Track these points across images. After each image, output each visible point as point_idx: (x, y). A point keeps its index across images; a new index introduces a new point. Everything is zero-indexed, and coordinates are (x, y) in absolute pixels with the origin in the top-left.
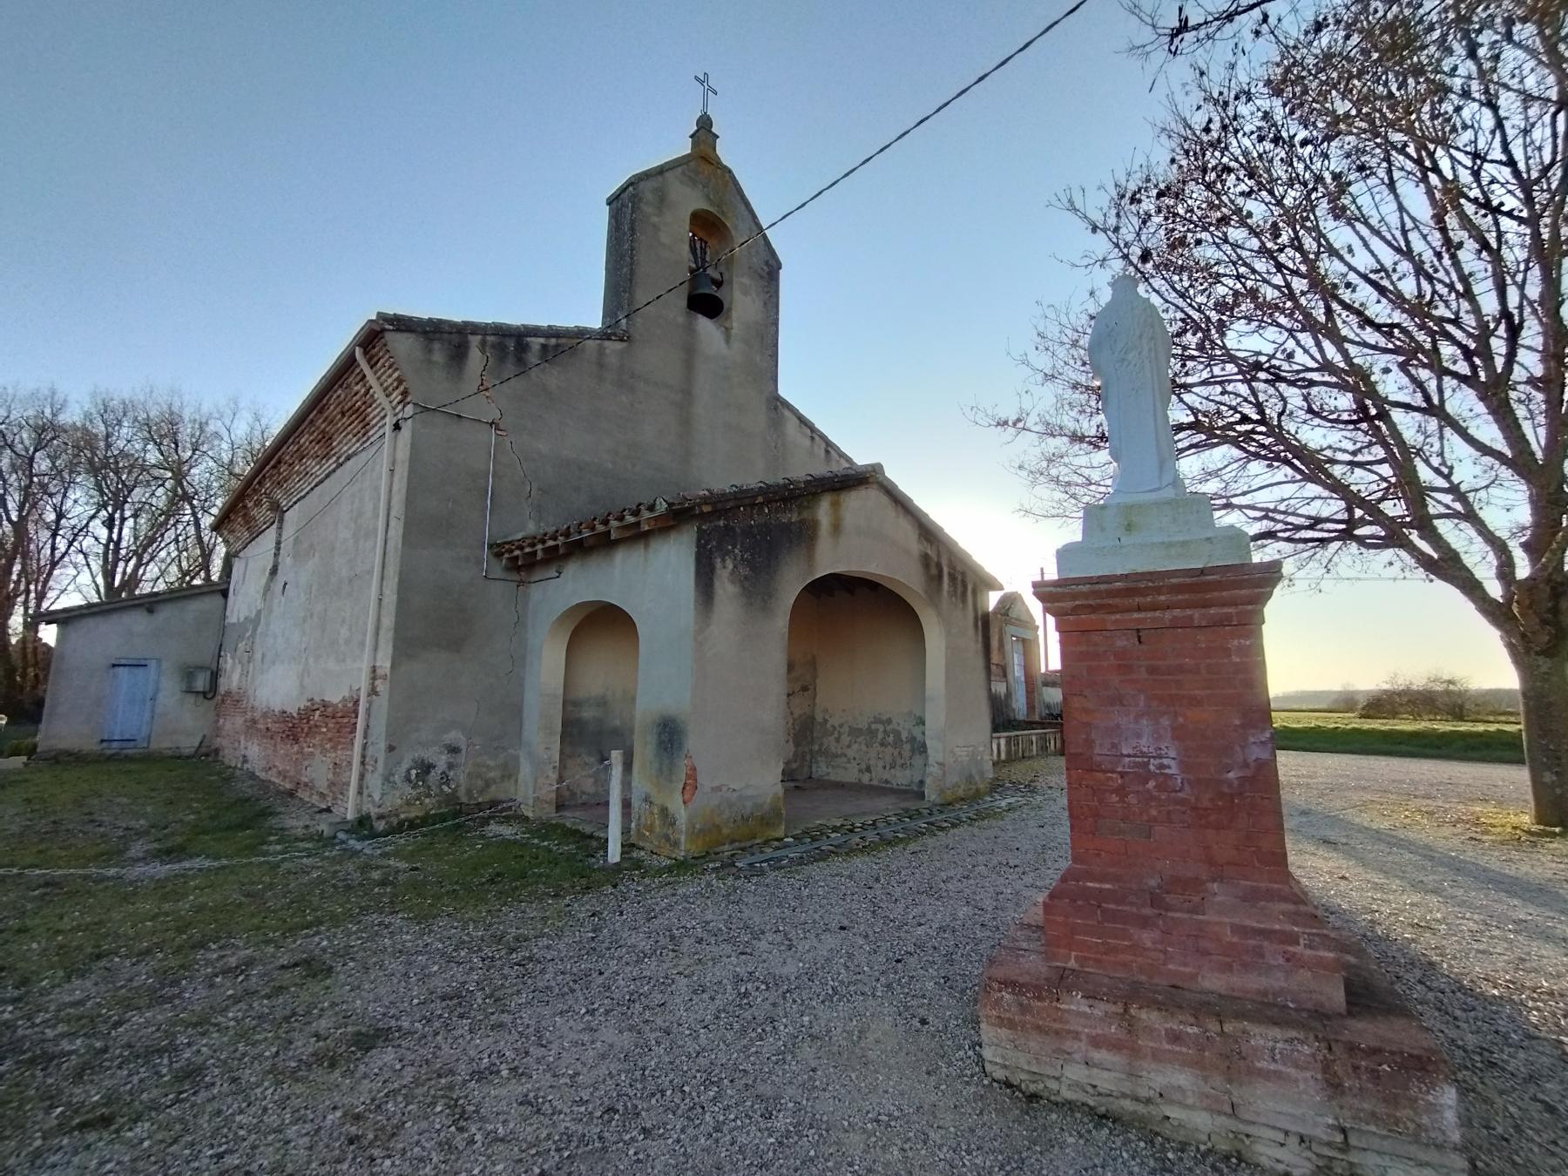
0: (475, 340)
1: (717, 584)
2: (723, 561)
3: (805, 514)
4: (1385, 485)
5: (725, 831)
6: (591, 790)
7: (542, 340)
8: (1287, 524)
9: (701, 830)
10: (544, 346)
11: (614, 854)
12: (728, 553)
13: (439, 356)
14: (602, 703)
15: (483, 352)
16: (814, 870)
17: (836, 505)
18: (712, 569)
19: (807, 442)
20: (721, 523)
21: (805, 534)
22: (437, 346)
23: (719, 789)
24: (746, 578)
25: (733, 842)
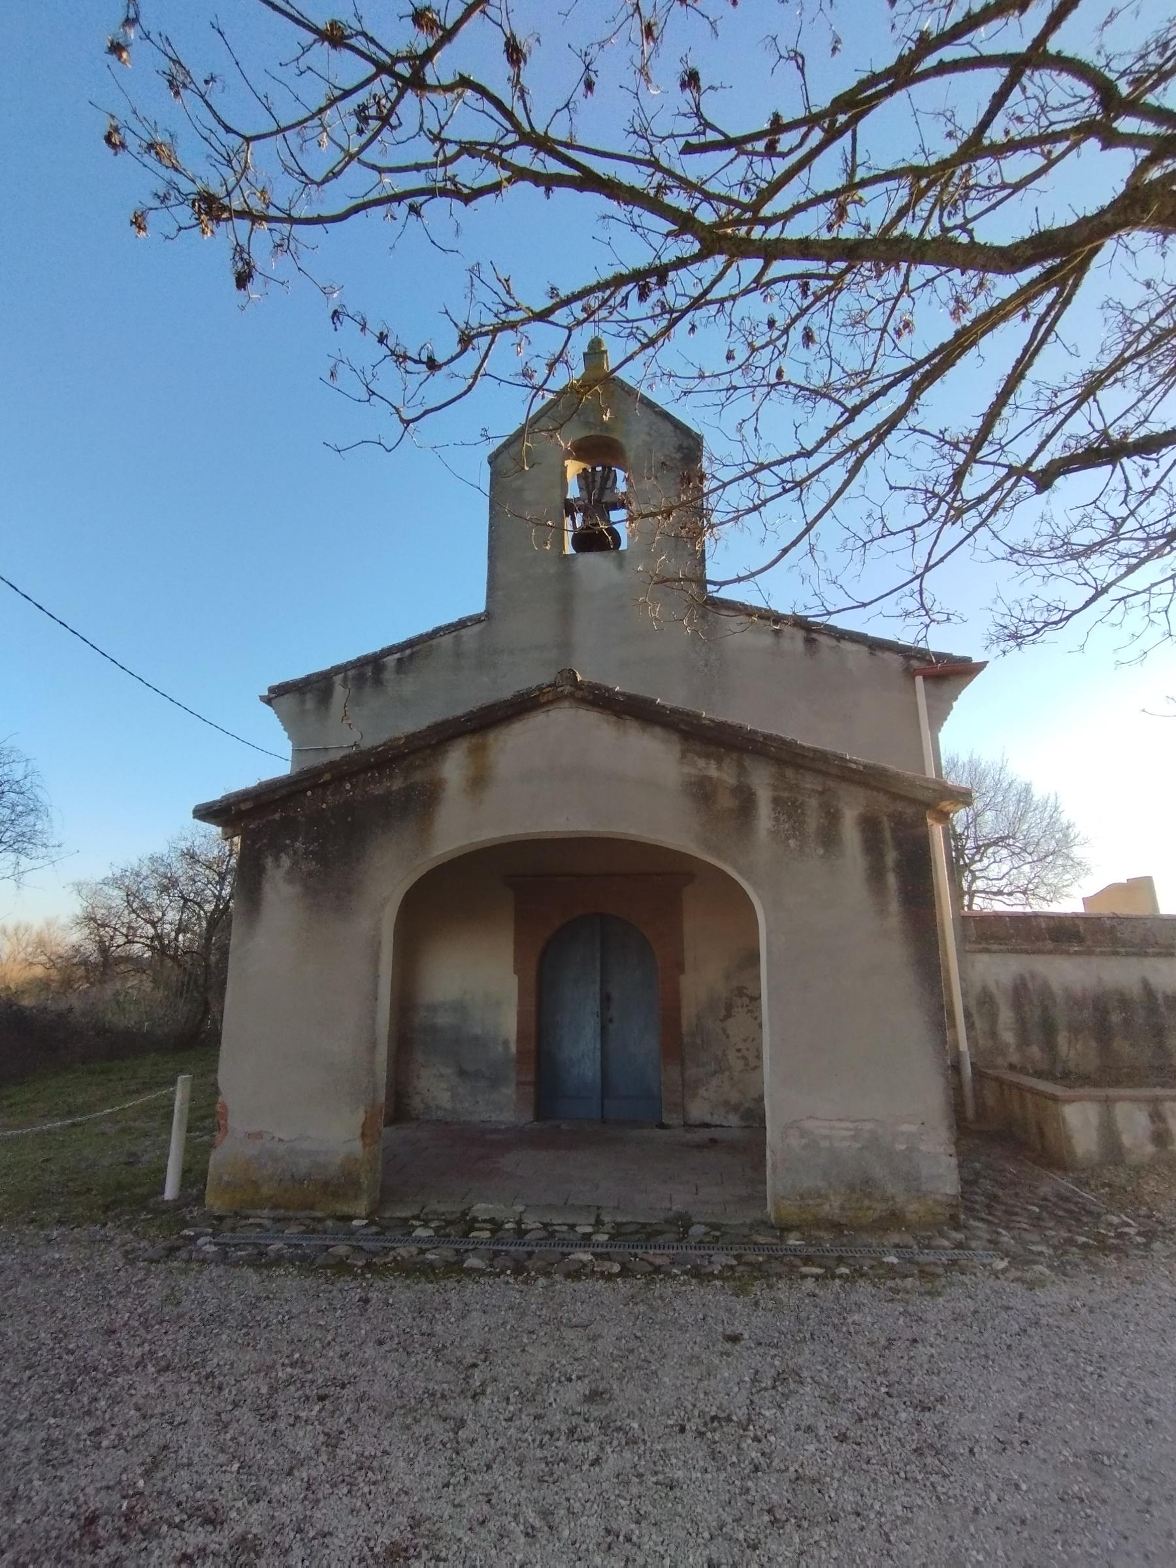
0: (338, 679)
1: (267, 888)
2: (277, 859)
3: (418, 777)
4: (349, 68)
5: (265, 1191)
6: (448, 1106)
7: (398, 656)
8: (855, 445)
9: (228, 1184)
10: (399, 660)
11: (170, 1191)
12: (283, 849)
13: (310, 704)
14: (459, 1007)
15: (345, 686)
16: (288, 1282)
17: (478, 752)
18: (261, 870)
19: (767, 640)
20: (277, 816)
21: (422, 802)
22: (309, 696)
23: (259, 1135)
24: (310, 874)
25: (275, 1207)
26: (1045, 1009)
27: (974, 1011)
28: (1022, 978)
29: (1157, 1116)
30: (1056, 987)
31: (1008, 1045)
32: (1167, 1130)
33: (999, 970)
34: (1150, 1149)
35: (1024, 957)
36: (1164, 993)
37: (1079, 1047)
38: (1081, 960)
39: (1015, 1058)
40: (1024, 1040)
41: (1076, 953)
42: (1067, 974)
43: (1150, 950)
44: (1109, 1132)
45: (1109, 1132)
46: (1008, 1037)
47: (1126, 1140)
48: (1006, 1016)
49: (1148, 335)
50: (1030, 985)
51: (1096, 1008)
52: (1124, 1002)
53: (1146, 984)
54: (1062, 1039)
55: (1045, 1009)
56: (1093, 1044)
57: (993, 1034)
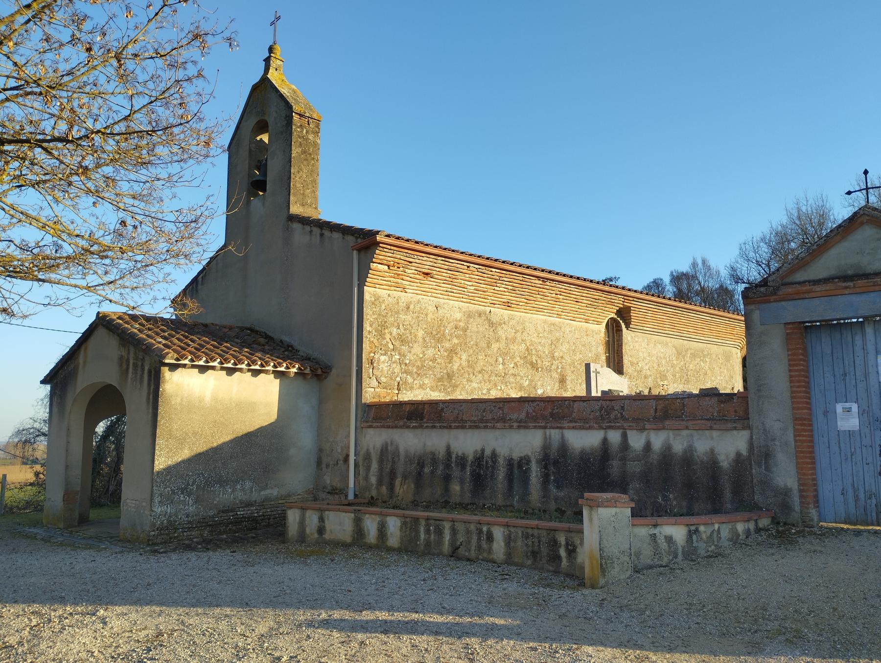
26: (394, 462)
27: (361, 464)
28: (387, 444)
29: (322, 519)
30: (402, 450)
31: (372, 485)
32: (324, 527)
33: (375, 438)
34: (316, 536)
35: (390, 430)
36: (406, 456)
37: (405, 487)
38: (418, 431)
39: (374, 493)
40: (380, 482)
41: (414, 427)
42: (411, 441)
43: (453, 425)
44: (302, 524)
45: (302, 524)
46: (373, 480)
47: (308, 531)
48: (375, 466)
49: (103, 262)
50: (389, 448)
51: (418, 464)
52: (434, 460)
53: (448, 448)
54: (398, 482)
55: (394, 462)
56: (413, 486)
57: (366, 478)
